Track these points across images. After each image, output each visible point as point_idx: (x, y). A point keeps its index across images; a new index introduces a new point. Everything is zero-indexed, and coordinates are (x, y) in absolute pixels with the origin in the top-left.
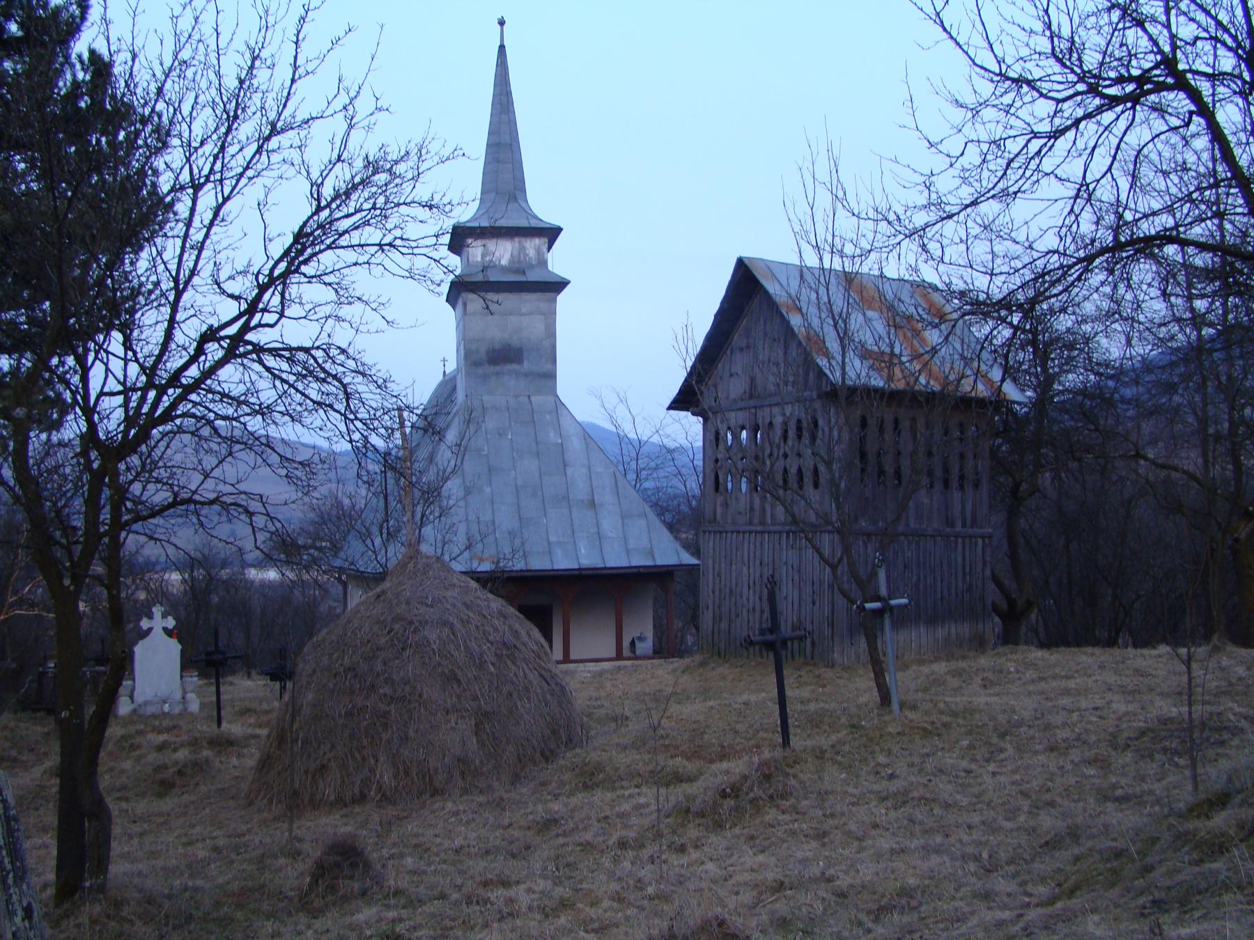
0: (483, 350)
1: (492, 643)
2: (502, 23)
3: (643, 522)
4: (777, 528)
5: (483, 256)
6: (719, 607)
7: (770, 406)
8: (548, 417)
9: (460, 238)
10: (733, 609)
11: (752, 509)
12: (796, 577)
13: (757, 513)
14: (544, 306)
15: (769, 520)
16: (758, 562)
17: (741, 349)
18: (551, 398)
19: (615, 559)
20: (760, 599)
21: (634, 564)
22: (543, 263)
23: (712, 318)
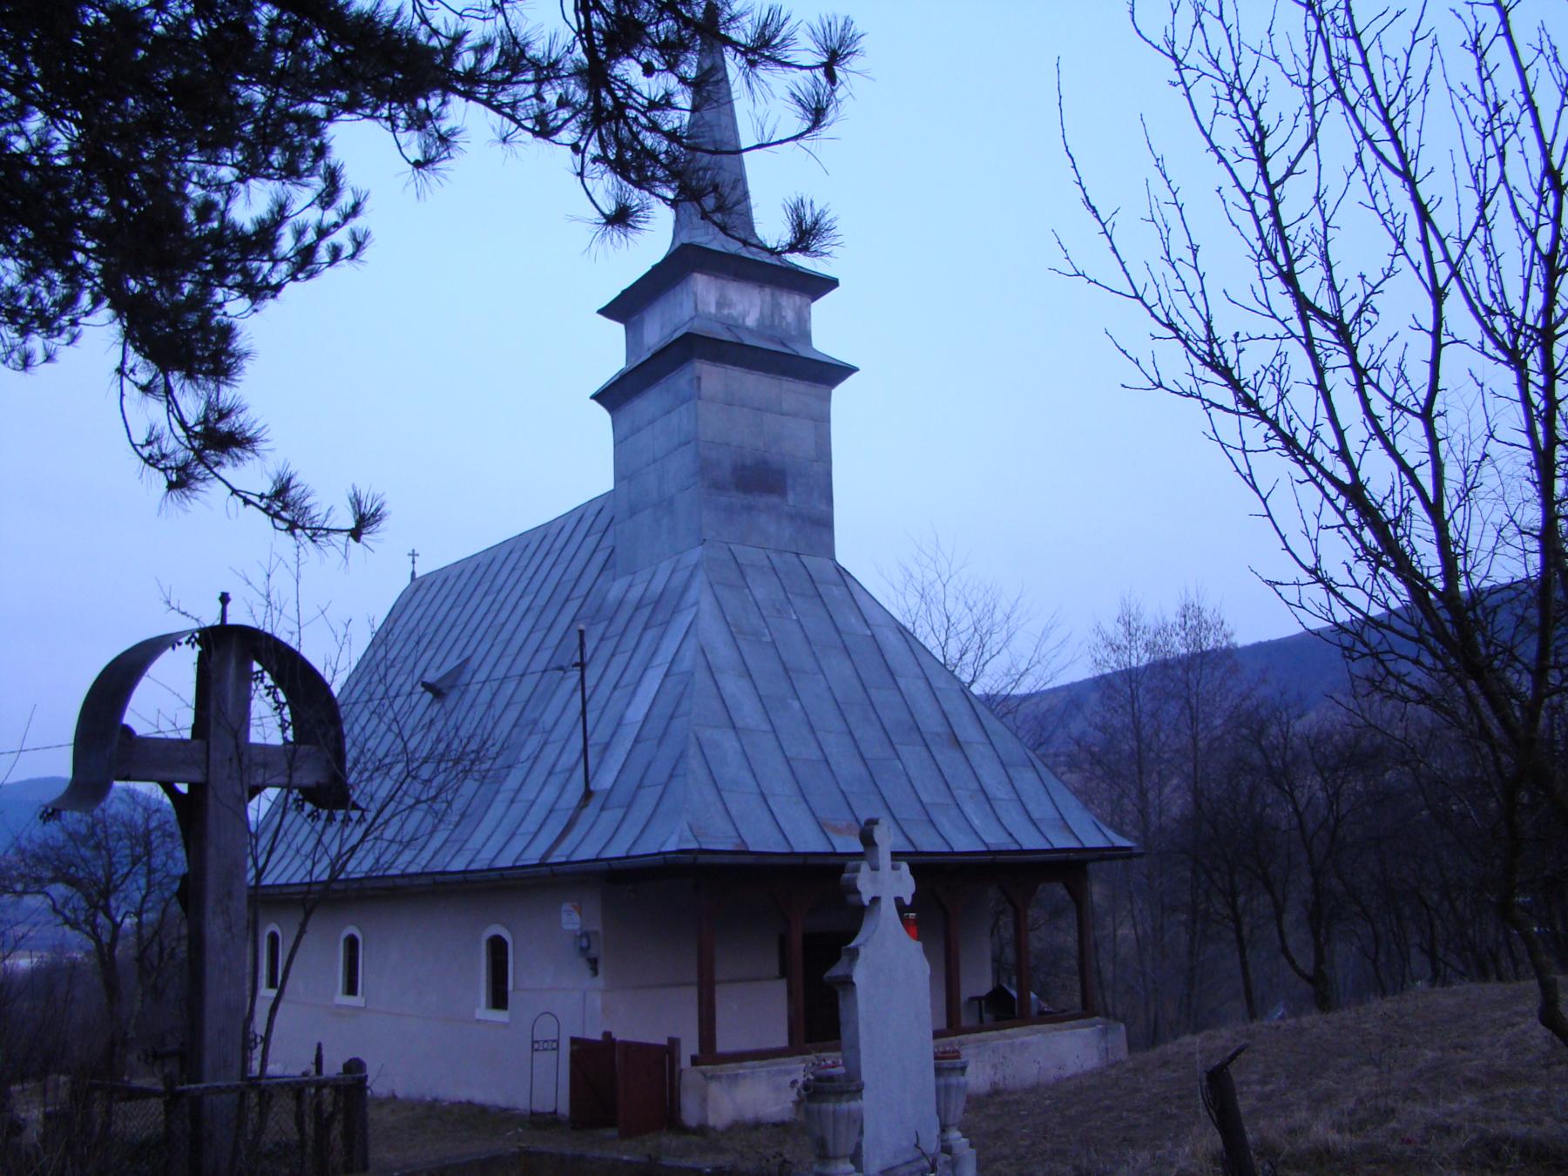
5: (720, 305)
22: (806, 336)
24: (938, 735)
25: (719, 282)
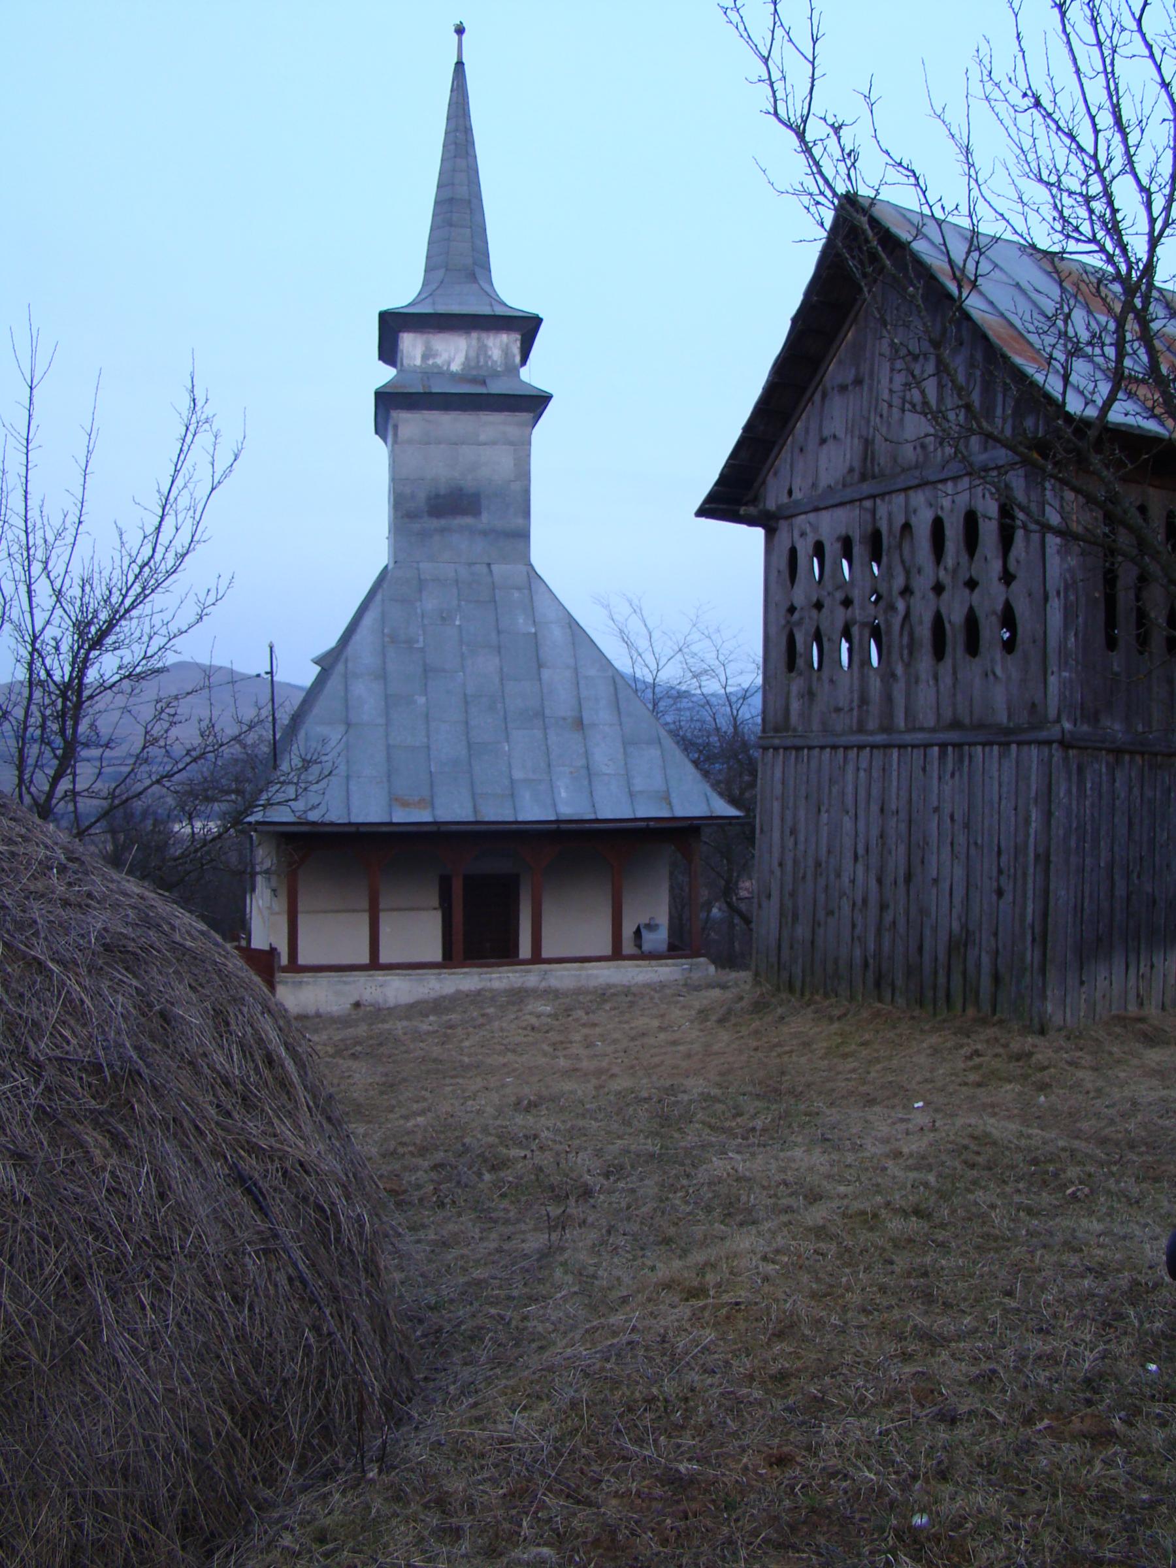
0: (422, 496)
1: (36, 1069)
2: (460, 31)
3: (655, 752)
4: (919, 737)
5: (425, 357)
6: (792, 894)
7: (906, 490)
8: (516, 595)
9: (392, 326)
10: (822, 897)
11: (864, 700)
12: (961, 839)
13: (875, 709)
14: (513, 431)
15: (900, 722)
16: (875, 808)
17: (843, 388)
18: (522, 568)
19: (612, 805)
20: (880, 881)
21: (640, 814)
23: (786, 326)
24: (564, 719)
25: (425, 336)
